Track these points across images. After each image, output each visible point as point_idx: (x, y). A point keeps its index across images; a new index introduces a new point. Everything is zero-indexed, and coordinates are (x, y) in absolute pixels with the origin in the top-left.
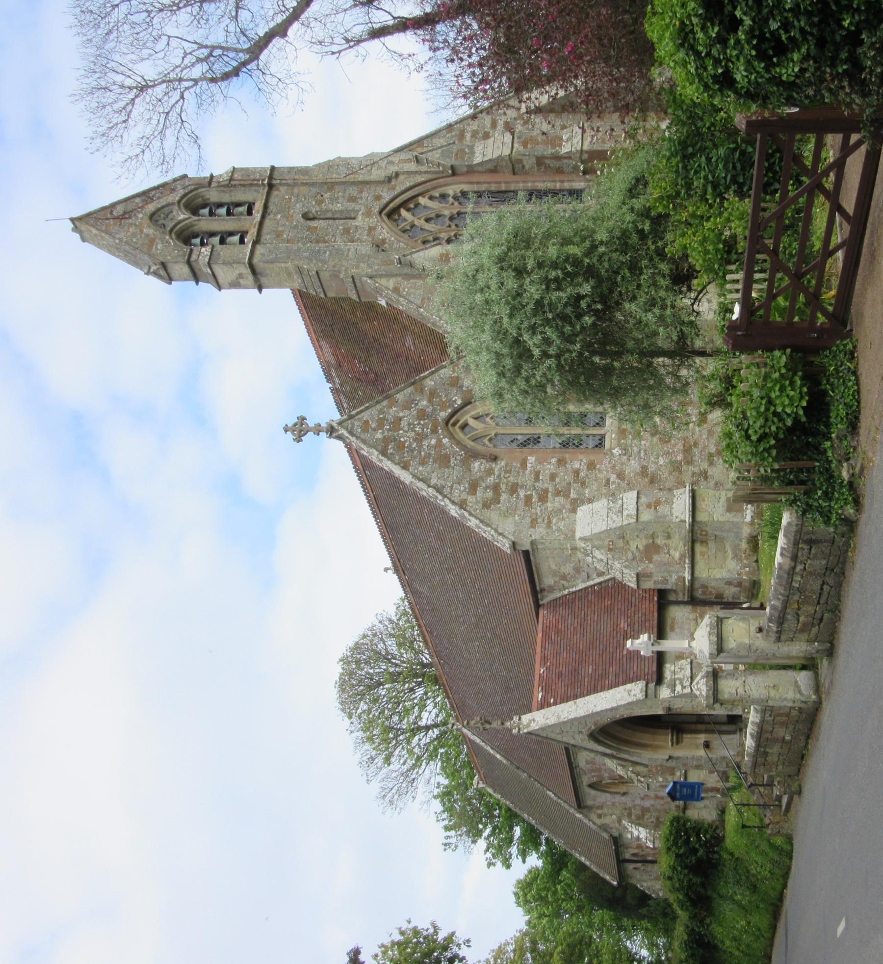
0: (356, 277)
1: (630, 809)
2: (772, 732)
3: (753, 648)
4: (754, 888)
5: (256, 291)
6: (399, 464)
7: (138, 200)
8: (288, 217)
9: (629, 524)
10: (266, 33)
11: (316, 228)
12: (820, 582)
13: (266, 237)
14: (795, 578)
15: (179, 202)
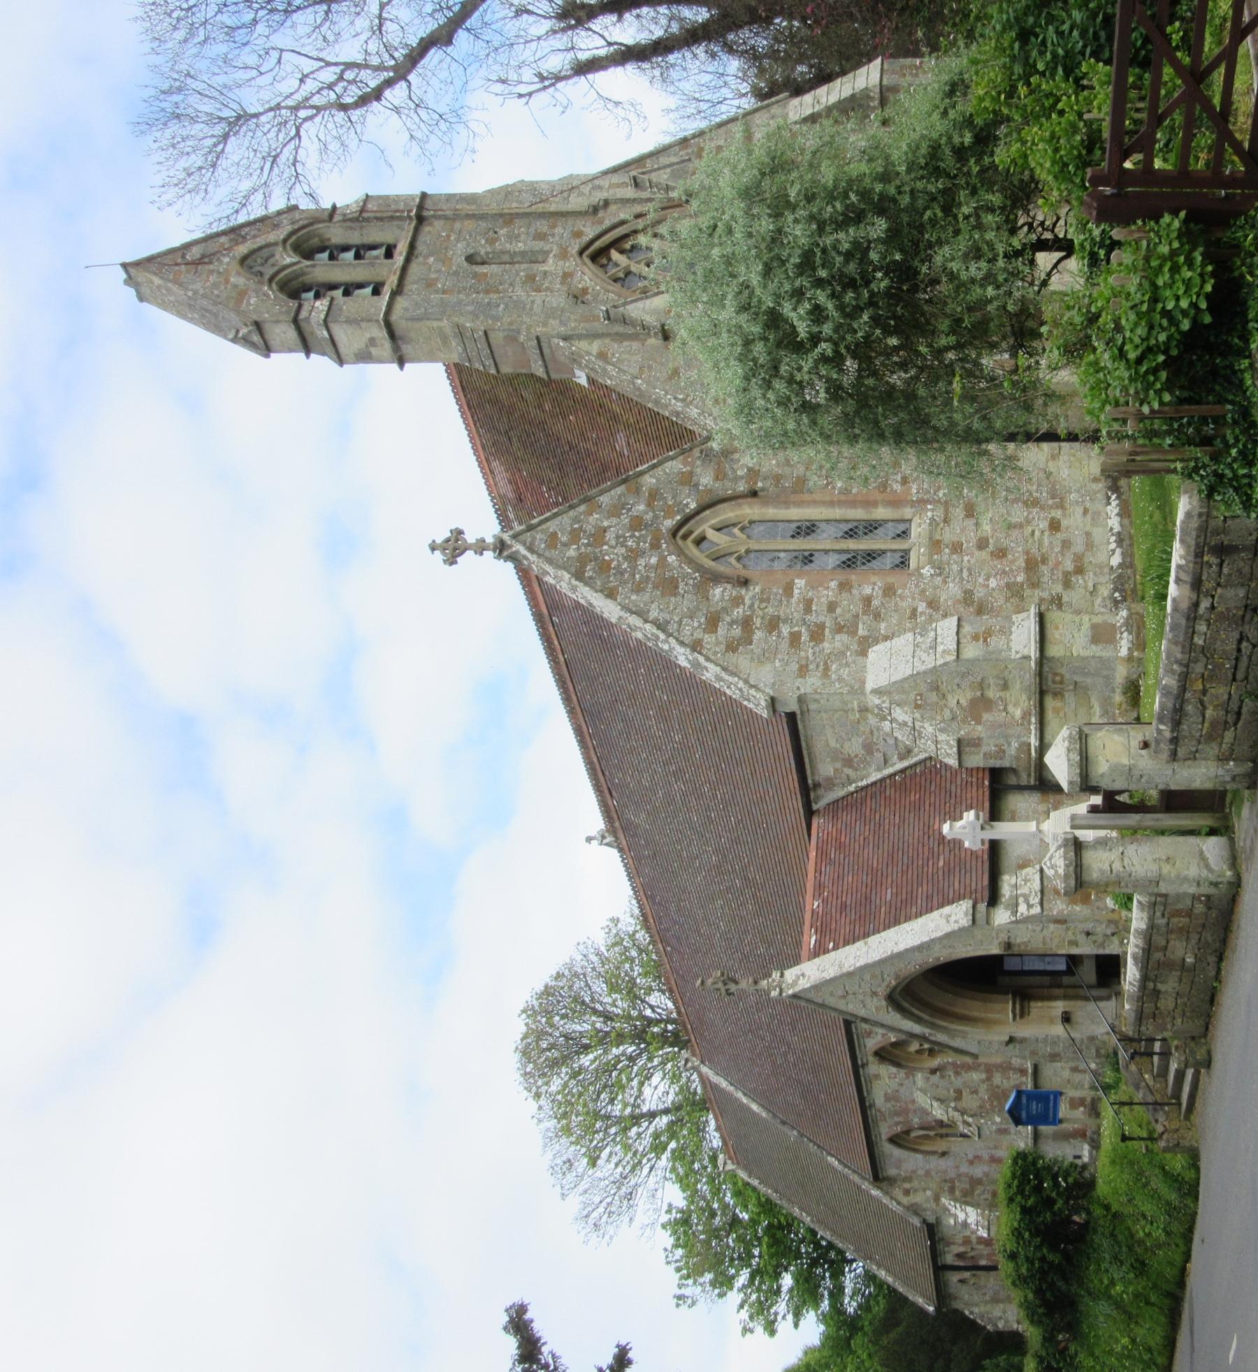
0: (542, 340)
1: (952, 1181)
2: (1166, 948)
3: (1136, 773)
4: (1141, 1267)
5: (395, 366)
6: (601, 591)
7: (223, 239)
8: (445, 261)
9: (946, 664)
10: (422, 39)
11: (485, 275)
12: (1236, 635)
13: (410, 286)
14: (1198, 628)
15: (285, 241)
